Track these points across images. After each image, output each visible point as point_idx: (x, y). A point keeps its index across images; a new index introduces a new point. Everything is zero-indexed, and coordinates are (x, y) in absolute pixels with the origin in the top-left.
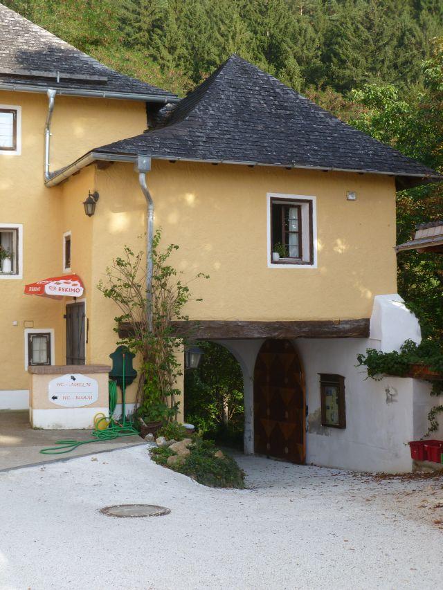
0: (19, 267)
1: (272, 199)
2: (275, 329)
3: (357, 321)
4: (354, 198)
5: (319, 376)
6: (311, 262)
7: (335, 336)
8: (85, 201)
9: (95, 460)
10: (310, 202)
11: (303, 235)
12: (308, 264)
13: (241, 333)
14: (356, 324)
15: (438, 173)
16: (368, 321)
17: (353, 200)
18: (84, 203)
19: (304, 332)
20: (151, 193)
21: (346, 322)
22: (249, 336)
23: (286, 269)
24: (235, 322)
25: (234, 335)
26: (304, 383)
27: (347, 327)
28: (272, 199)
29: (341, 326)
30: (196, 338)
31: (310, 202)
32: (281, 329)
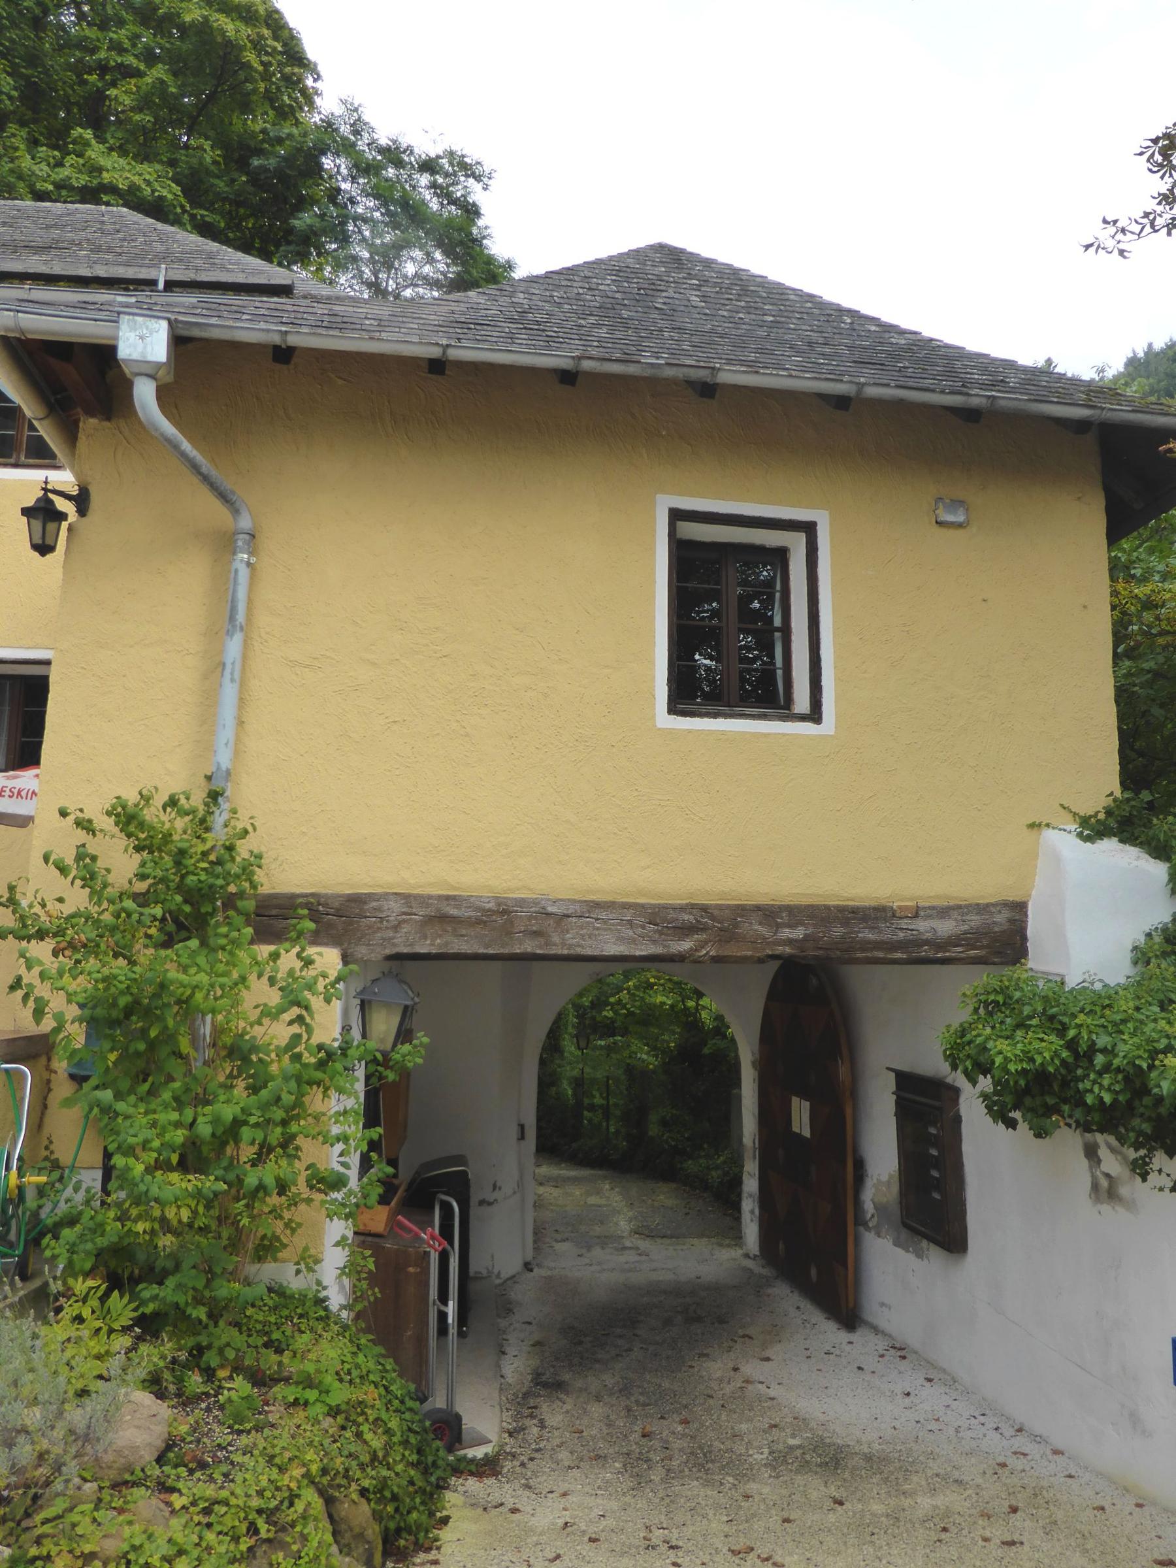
0: (824, 664)
1: (676, 515)
2: (686, 930)
3: (982, 909)
4: (961, 518)
5: (893, 1075)
6: (815, 715)
7: (899, 955)
8: (30, 503)
9: (522, 1137)
10: (809, 529)
11: (793, 638)
12: (803, 718)
13: (556, 939)
14: (975, 920)
15: (171, 35)
16: (1020, 908)
17: (960, 526)
18: (26, 512)
19: (790, 942)
20: (228, 483)
21: (943, 912)
22: (589, 952)
23: (723, 733)
24: (535, 902)
25: (529, 946)
26: (854, 1094)
27: (945, 928)
28: (676, 515)
29: (922, 926)
30: (388, 952)
31: (809, 529)
32: (704, 929)
